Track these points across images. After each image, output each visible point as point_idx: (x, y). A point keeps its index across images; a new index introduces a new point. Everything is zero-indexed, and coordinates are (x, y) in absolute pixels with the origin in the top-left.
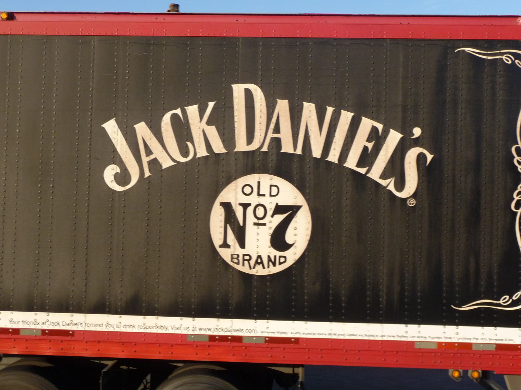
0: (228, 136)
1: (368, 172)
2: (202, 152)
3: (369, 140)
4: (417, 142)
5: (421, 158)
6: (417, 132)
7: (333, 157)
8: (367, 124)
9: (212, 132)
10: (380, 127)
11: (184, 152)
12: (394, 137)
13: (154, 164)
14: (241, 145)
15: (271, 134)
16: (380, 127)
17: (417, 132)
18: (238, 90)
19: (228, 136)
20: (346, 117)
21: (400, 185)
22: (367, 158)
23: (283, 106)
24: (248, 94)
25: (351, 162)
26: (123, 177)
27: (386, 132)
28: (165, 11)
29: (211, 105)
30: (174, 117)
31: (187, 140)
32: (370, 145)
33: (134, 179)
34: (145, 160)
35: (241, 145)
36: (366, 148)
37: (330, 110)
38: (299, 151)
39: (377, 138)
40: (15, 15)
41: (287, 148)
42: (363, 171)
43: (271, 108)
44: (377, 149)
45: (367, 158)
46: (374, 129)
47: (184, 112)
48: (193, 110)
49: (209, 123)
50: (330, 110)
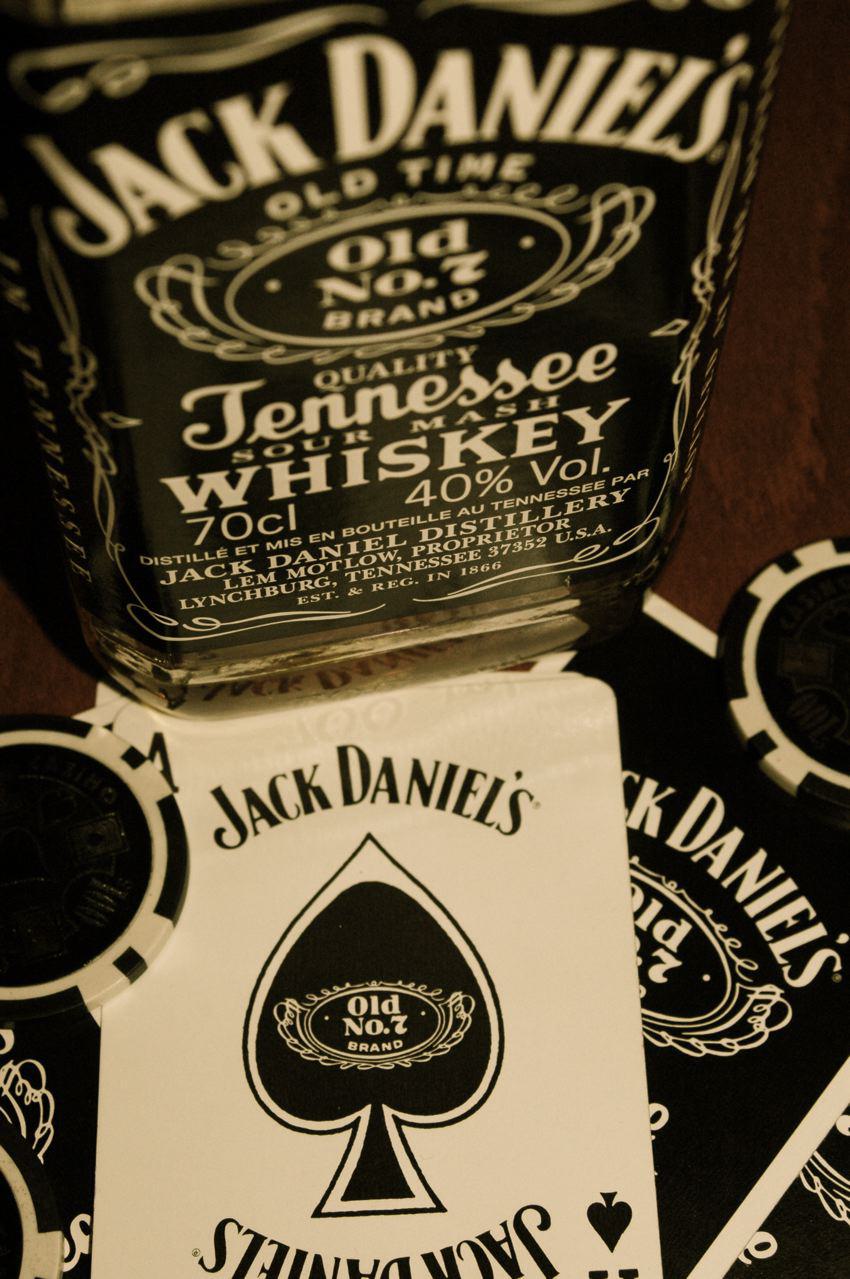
1: (772, 942)
3: (794, 918)
5: (830, 962)
6: (843, 939)
7: (752, 910)
8: (802, 904)
9: (656, 815)
10: (813, 914)
12: (818, 931)
14: (675, 841)
15: (708, 851)
16: (813, 914)
17: (843, 939)
18: (705, 795)
20: (790, 886)
22: (780, 932)
23: (735, 837)
25: (763, 926)
27: (814, 923)
28: (627, 814)
29: (670, 791)
31: (576, 443)
32: (791, 923)
34: (708, 851)
35: (675, 841)
36: (786, 922)
37: (779, 871)
40: (675, 950)
41: (715, 871)
42: (768, 938)
43: (723, 831)
45: (780, 932)
46: (806, 913)
47: (642, 782)
49: (658, 804)
50: (779, 871)
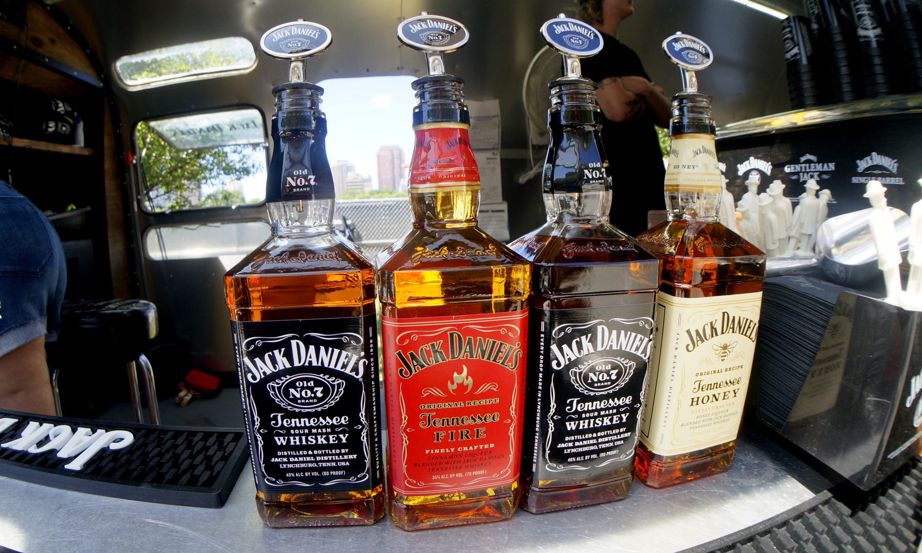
0: (291, 361)
2: (282, 367)
4: (363, 358)
5: (364, 363)
8: (639, 336)
9: (285, 359)
11: (275, 368)
13: (264, 373)
14: (296, 364)
19: (291, 361)
21: (357, 374)
24: (297, 344)
26: (559, 364)
30: (577, 342)
33: (563, 366)
35: (296, 364)
37: (330, 349)
38: (320, 365)
39: (641, 340)
41: (614, 348)
44: (348, 362)
45: (637, 349)
48: (583, 338)
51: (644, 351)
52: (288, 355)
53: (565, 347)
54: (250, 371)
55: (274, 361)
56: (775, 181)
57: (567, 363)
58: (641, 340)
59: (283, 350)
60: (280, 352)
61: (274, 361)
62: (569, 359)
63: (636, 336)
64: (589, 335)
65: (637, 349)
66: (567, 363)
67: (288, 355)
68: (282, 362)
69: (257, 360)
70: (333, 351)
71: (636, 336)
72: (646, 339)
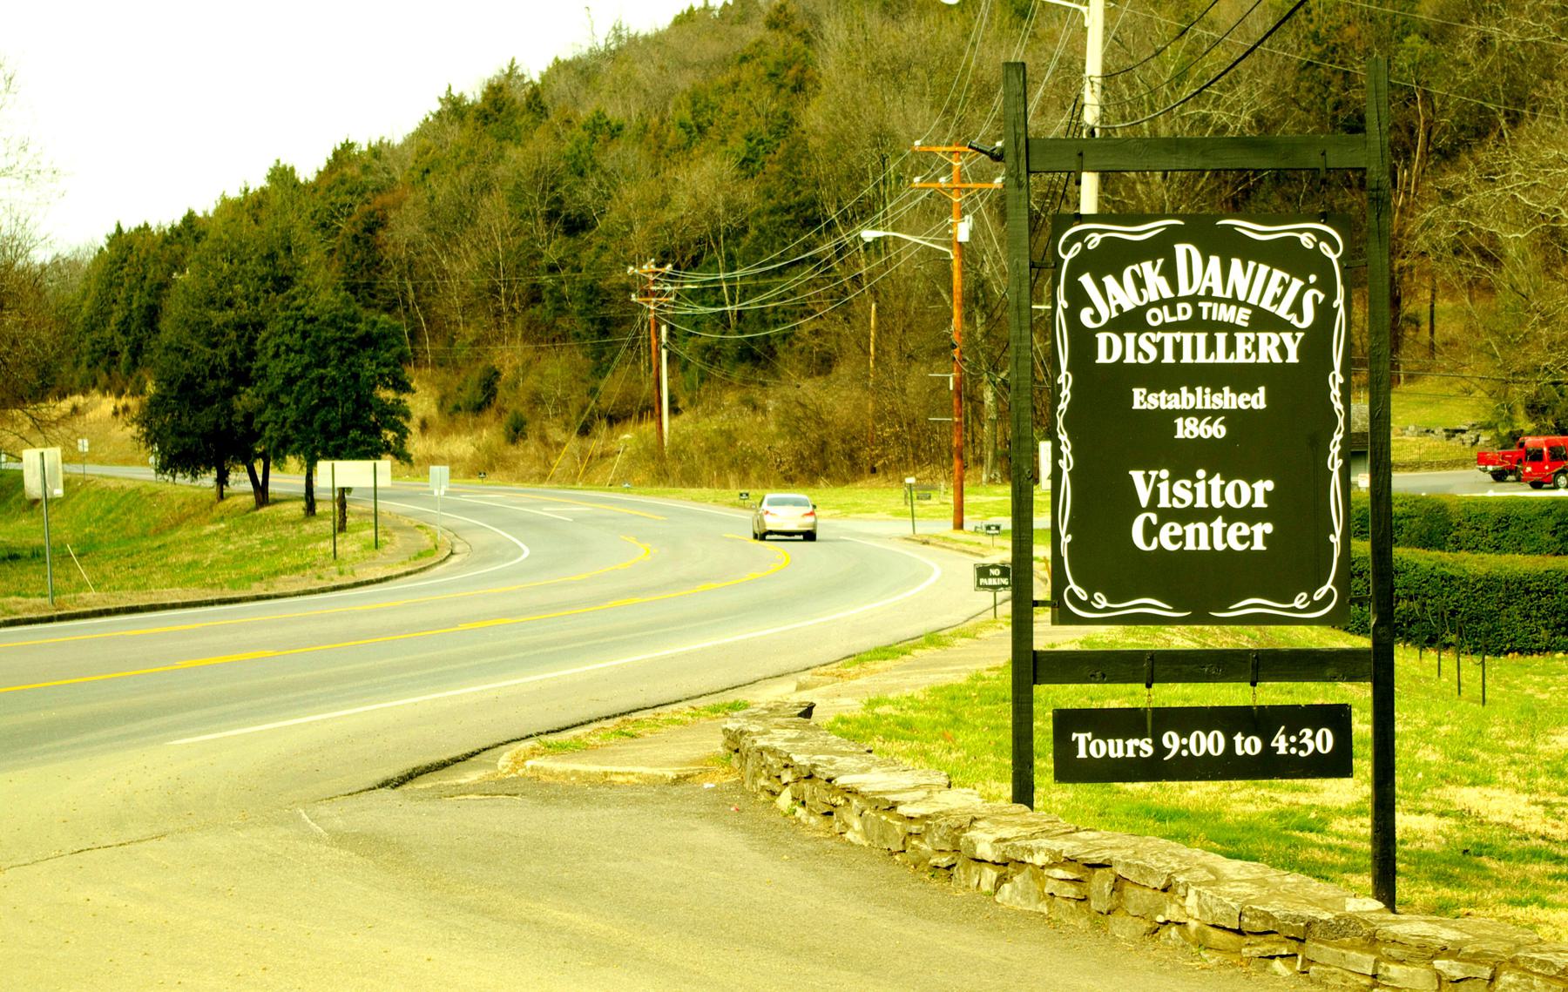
0: (1174, 285)
8: (1278, 275)
19: (1174, 285)
21: (1301, 319)
30: (1134, 273)
37: (1252, 264)
39: (1285, 285)
45: (1277, 300)
51: (1297, 308)
52: (1169, 272)
53: (1109, 280)
54: (1090, 303)
55: (1140, 283)
56: (312, 178)
57: (1115, 314)
58: (1285, 285)
59: (1160, 261)
60: (1154, 265)
61: (1140, 283)
62: (1119, 308)
63: (1270, 274)
64: (1160, 261)
65: (1277, 300)
66: (1115, 314)
67: (1169, 272)
68: (1157, 285)
69: (1109, 280)
70: (1256, 269)
71: (1270, 274)
72: (1297, 284)
